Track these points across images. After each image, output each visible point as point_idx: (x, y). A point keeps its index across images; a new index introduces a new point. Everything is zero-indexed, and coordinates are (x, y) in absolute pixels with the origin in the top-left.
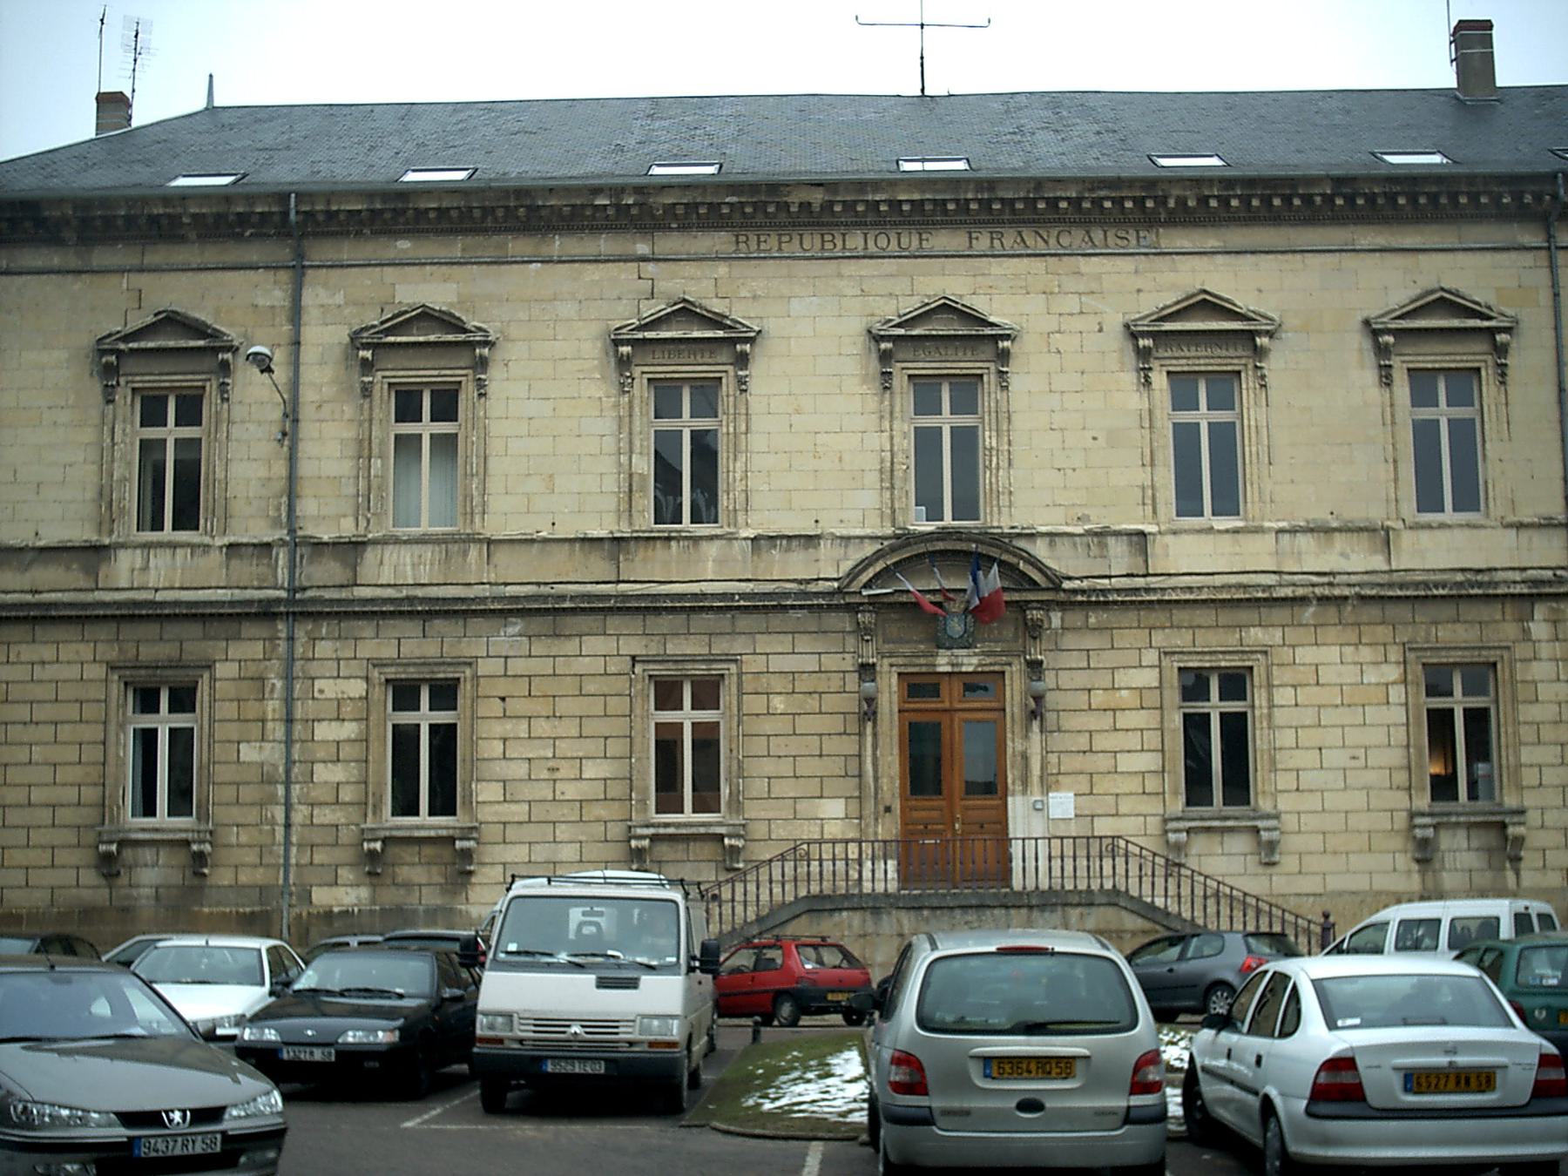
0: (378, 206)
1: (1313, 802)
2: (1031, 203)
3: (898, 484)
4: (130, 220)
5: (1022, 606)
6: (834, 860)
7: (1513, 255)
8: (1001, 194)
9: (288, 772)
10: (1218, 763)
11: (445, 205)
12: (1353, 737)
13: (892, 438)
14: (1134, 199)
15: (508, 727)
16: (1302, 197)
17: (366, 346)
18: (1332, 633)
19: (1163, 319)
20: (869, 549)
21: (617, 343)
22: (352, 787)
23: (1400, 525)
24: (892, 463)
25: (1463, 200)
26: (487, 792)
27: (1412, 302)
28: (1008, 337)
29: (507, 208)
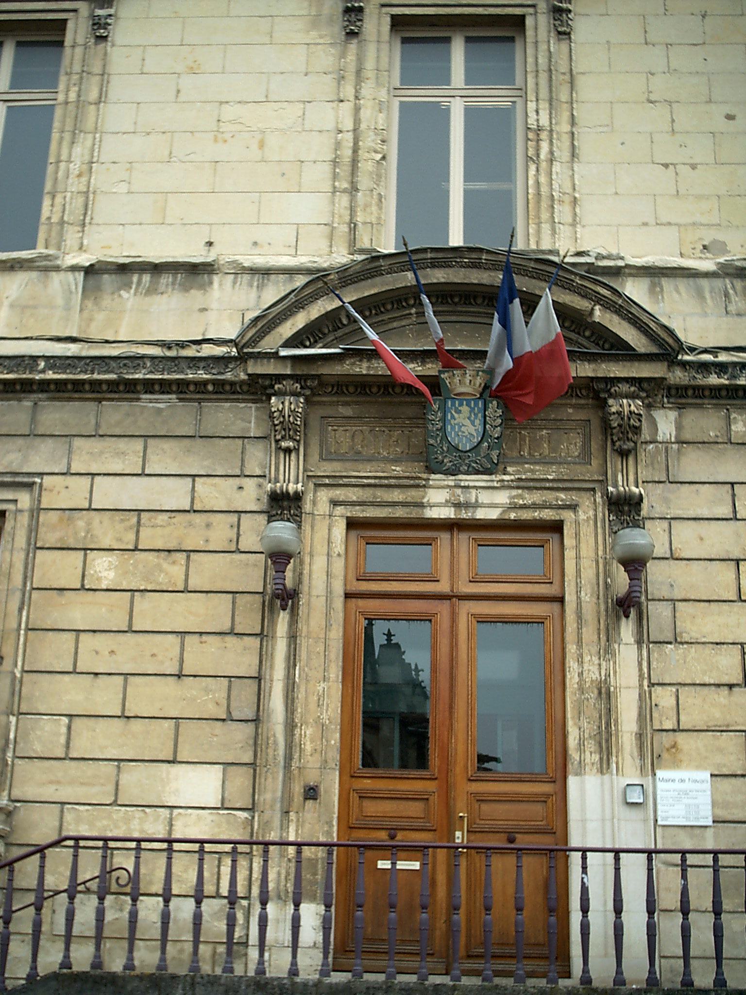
3: (364, 182)
5: (597, 392)
13: (357, 109)
24: (355, 150)
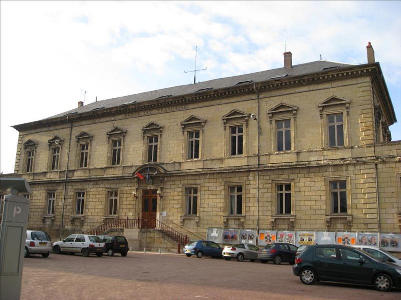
7: (251, 101)
18: (212, 180)
19: (187, 121)
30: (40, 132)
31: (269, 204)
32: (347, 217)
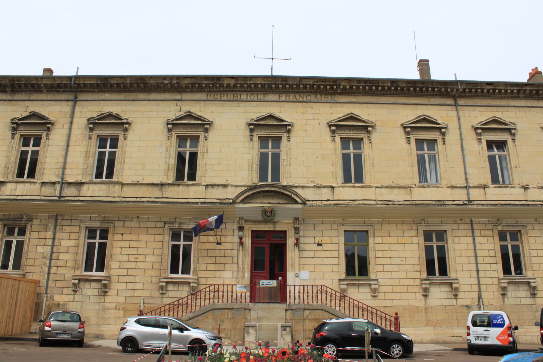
0: (99, 82)
1: (388, 275)
2: (298, 85)
4: (26, 85)
6: (228, 292)
8: (289, 83)
9: (51, 255)
10: (357, 265)
11: (119, 82)
12: (402, 254)
14: (330, 85)
15: (123, 244)
16: (381, 86)
17: (91, 123)
19: (339, 121)
20: (243, 189)
21: (168, 124)
22: (71, 261)
23: (414, 186)
25: (430, 89)
26: (115, 265)
27: (416, 118)
28: (290, 125)
29: (137, 83)
30: (9, 100)
31: (493, 260)
32: (371, 283)
